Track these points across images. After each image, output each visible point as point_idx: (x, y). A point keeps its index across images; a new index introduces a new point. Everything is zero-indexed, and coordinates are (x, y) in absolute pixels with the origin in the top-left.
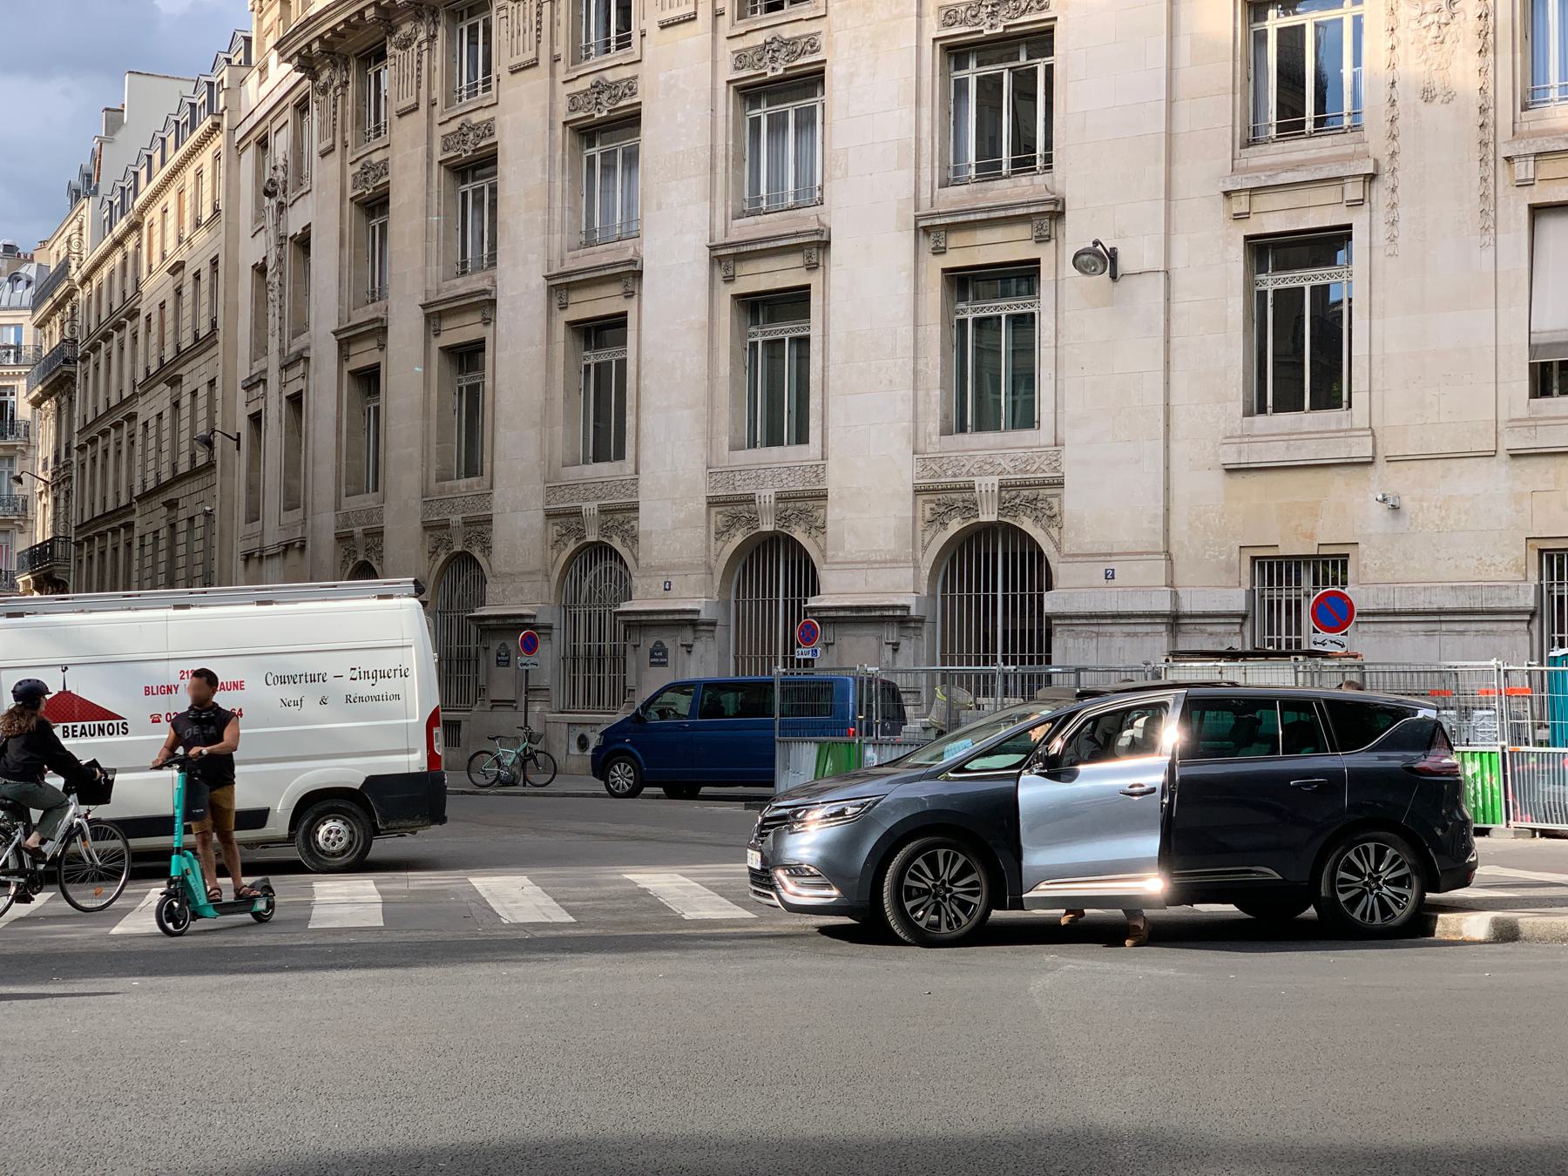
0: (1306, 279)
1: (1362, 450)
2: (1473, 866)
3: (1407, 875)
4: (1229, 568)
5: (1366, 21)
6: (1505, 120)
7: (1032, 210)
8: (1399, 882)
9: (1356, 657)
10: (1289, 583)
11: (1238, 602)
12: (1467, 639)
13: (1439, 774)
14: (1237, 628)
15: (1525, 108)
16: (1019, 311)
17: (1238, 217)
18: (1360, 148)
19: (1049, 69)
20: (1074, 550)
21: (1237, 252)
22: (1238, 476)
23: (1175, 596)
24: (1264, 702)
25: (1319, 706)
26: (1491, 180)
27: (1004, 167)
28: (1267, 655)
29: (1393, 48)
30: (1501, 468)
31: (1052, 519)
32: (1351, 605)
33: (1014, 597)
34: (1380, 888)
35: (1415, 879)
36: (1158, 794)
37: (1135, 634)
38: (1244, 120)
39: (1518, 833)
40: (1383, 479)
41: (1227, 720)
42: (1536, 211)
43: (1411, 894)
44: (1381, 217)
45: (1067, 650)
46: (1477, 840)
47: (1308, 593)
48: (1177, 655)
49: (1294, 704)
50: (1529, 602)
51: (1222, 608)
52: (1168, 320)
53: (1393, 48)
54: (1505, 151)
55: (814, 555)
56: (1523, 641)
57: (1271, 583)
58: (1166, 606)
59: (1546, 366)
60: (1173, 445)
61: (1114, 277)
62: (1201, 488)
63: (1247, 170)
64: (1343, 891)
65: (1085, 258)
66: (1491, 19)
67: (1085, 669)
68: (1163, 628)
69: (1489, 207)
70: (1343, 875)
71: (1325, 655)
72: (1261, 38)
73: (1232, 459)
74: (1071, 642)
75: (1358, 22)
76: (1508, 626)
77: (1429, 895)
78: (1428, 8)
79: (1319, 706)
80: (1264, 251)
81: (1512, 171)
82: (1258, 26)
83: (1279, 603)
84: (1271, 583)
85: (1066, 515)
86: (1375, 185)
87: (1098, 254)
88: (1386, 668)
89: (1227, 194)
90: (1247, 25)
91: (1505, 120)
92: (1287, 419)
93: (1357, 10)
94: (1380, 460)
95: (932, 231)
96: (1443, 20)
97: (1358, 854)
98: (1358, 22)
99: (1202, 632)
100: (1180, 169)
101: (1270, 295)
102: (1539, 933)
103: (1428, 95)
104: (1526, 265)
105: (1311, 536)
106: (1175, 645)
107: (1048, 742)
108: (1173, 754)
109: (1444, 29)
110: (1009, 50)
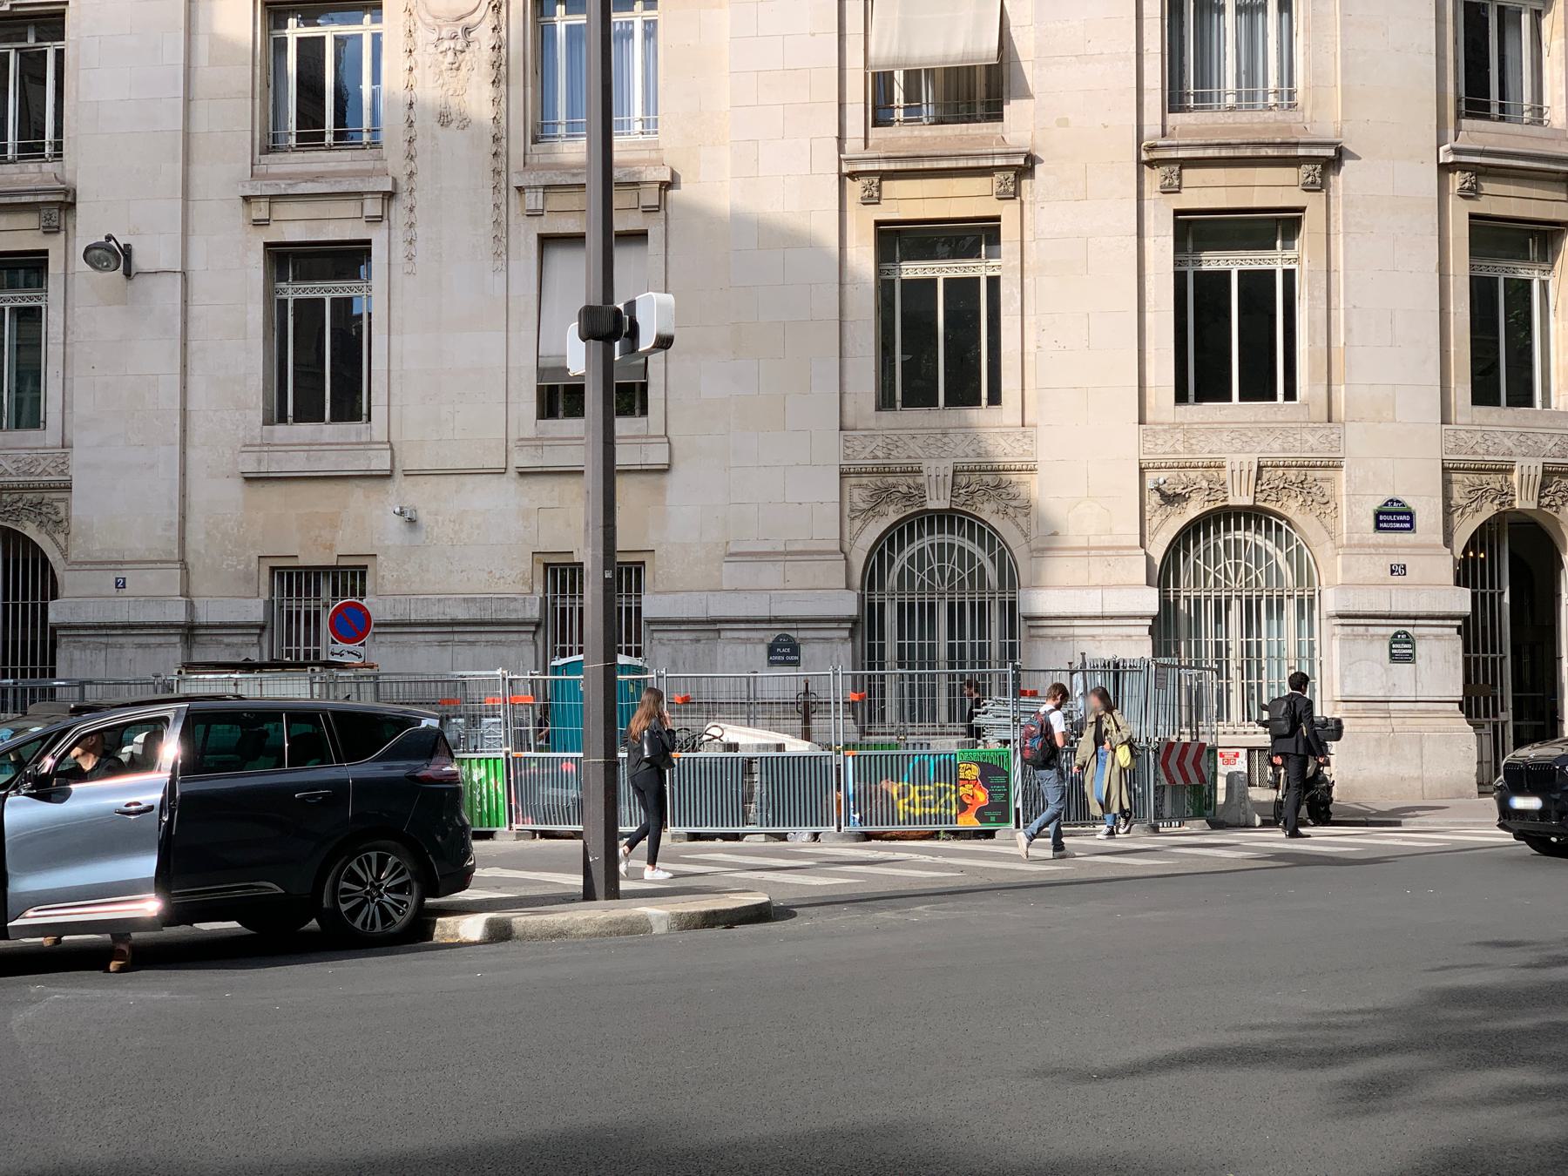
0: (327, 291)
1: (381, 463)
2: (471, 870)
3: (408, 882)
4: (247, 578)
5: (385, 40)
6: (516, 150)
7: (41, 199)
8: (399, 889)
9: (372, 667)
10: (308, 593)
11: (255, 611)
12: (477, 649)
13: (441, 782)
14: (255, 639)
15: (535, 141)
16: (24, 304)
17: (257, 223)
18: (378, 165)
19: (60, 54)
20: (82, 558)
21: (257, 259)
22: (258, 485)
23: (191, 607)
24: (268, 715)
25: (325, 717)
26: (503, 208)
27: (10, 151)
28: (283, 666)
29: (411, 69)
30: (509, 486)
31: (59, 524)
32: (367, 616)
33: (15, 607)
34: (381, 896)
35: (415, 886)
36: (156, 812)
37: (148, 646)
38: (264, 127)
39: (520, 835)
40: (402, 493)
41: (223, 735)
42: (545, 241)
43: (411, 900)
44: (399, 235)
45: (72, 662)
46: (475, 844)
47: (328, 603)
48: (191, 667)
49: (300, 716)
50: (534, 613)
51: (241, 619)
52: (185, 323)
53: (411, 69)
54: (516, 181)
55: (53, 555)
56: (528, 652)
57: (290, 593)
58: (179, 615)
59: (553, 389)
60: (190, 452)
61: (128, 274)
62: (218, 496)
63: (266, 176)
64: (345, 901)
65: (97, 252)
66: (503, 51)
67: (90, 683)
68: (177, 639)
69: (501, 234)
70: (346, 885)
71: (341, 666)
72: (281, 45)
73: (251, 467)
74: (77, 654)
75: (376, 38)
76: (514, 637)
77: (429, 901)
78: (444, 34)
79: (325, 717)
80: (285, 259)
81: (522, 201)
82: (278, 34)
83: (298, 613)
84: (290, 593)
85: (73, 522)
86: (393, 203)
87: (110, 250)
88: (399, 678)
89: (246, 199)
90: (267, 31)
91: (516, 150)
92: (306, 430)
93: (650, 15)
94: (398, 473)
95: (260, 203)
96: (459, 48)
97: (360, 864)
98: (376, 38)
99: (219, 643)
100: (198, 169)
101: (290, 305)
102: (530, 931)
103: (444, 119)
104: (535, 292)
105: (331, 547)
106: (190, 656)
107: (38, 761)
108: (174, 770)
109: (460, 57)
110: (19, 30)
